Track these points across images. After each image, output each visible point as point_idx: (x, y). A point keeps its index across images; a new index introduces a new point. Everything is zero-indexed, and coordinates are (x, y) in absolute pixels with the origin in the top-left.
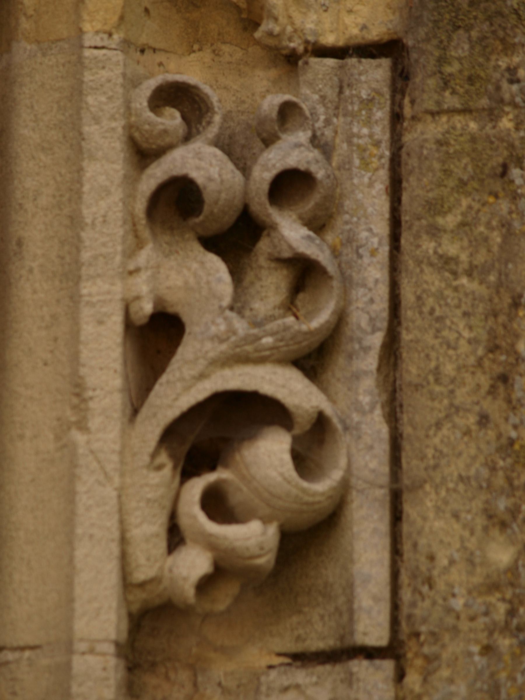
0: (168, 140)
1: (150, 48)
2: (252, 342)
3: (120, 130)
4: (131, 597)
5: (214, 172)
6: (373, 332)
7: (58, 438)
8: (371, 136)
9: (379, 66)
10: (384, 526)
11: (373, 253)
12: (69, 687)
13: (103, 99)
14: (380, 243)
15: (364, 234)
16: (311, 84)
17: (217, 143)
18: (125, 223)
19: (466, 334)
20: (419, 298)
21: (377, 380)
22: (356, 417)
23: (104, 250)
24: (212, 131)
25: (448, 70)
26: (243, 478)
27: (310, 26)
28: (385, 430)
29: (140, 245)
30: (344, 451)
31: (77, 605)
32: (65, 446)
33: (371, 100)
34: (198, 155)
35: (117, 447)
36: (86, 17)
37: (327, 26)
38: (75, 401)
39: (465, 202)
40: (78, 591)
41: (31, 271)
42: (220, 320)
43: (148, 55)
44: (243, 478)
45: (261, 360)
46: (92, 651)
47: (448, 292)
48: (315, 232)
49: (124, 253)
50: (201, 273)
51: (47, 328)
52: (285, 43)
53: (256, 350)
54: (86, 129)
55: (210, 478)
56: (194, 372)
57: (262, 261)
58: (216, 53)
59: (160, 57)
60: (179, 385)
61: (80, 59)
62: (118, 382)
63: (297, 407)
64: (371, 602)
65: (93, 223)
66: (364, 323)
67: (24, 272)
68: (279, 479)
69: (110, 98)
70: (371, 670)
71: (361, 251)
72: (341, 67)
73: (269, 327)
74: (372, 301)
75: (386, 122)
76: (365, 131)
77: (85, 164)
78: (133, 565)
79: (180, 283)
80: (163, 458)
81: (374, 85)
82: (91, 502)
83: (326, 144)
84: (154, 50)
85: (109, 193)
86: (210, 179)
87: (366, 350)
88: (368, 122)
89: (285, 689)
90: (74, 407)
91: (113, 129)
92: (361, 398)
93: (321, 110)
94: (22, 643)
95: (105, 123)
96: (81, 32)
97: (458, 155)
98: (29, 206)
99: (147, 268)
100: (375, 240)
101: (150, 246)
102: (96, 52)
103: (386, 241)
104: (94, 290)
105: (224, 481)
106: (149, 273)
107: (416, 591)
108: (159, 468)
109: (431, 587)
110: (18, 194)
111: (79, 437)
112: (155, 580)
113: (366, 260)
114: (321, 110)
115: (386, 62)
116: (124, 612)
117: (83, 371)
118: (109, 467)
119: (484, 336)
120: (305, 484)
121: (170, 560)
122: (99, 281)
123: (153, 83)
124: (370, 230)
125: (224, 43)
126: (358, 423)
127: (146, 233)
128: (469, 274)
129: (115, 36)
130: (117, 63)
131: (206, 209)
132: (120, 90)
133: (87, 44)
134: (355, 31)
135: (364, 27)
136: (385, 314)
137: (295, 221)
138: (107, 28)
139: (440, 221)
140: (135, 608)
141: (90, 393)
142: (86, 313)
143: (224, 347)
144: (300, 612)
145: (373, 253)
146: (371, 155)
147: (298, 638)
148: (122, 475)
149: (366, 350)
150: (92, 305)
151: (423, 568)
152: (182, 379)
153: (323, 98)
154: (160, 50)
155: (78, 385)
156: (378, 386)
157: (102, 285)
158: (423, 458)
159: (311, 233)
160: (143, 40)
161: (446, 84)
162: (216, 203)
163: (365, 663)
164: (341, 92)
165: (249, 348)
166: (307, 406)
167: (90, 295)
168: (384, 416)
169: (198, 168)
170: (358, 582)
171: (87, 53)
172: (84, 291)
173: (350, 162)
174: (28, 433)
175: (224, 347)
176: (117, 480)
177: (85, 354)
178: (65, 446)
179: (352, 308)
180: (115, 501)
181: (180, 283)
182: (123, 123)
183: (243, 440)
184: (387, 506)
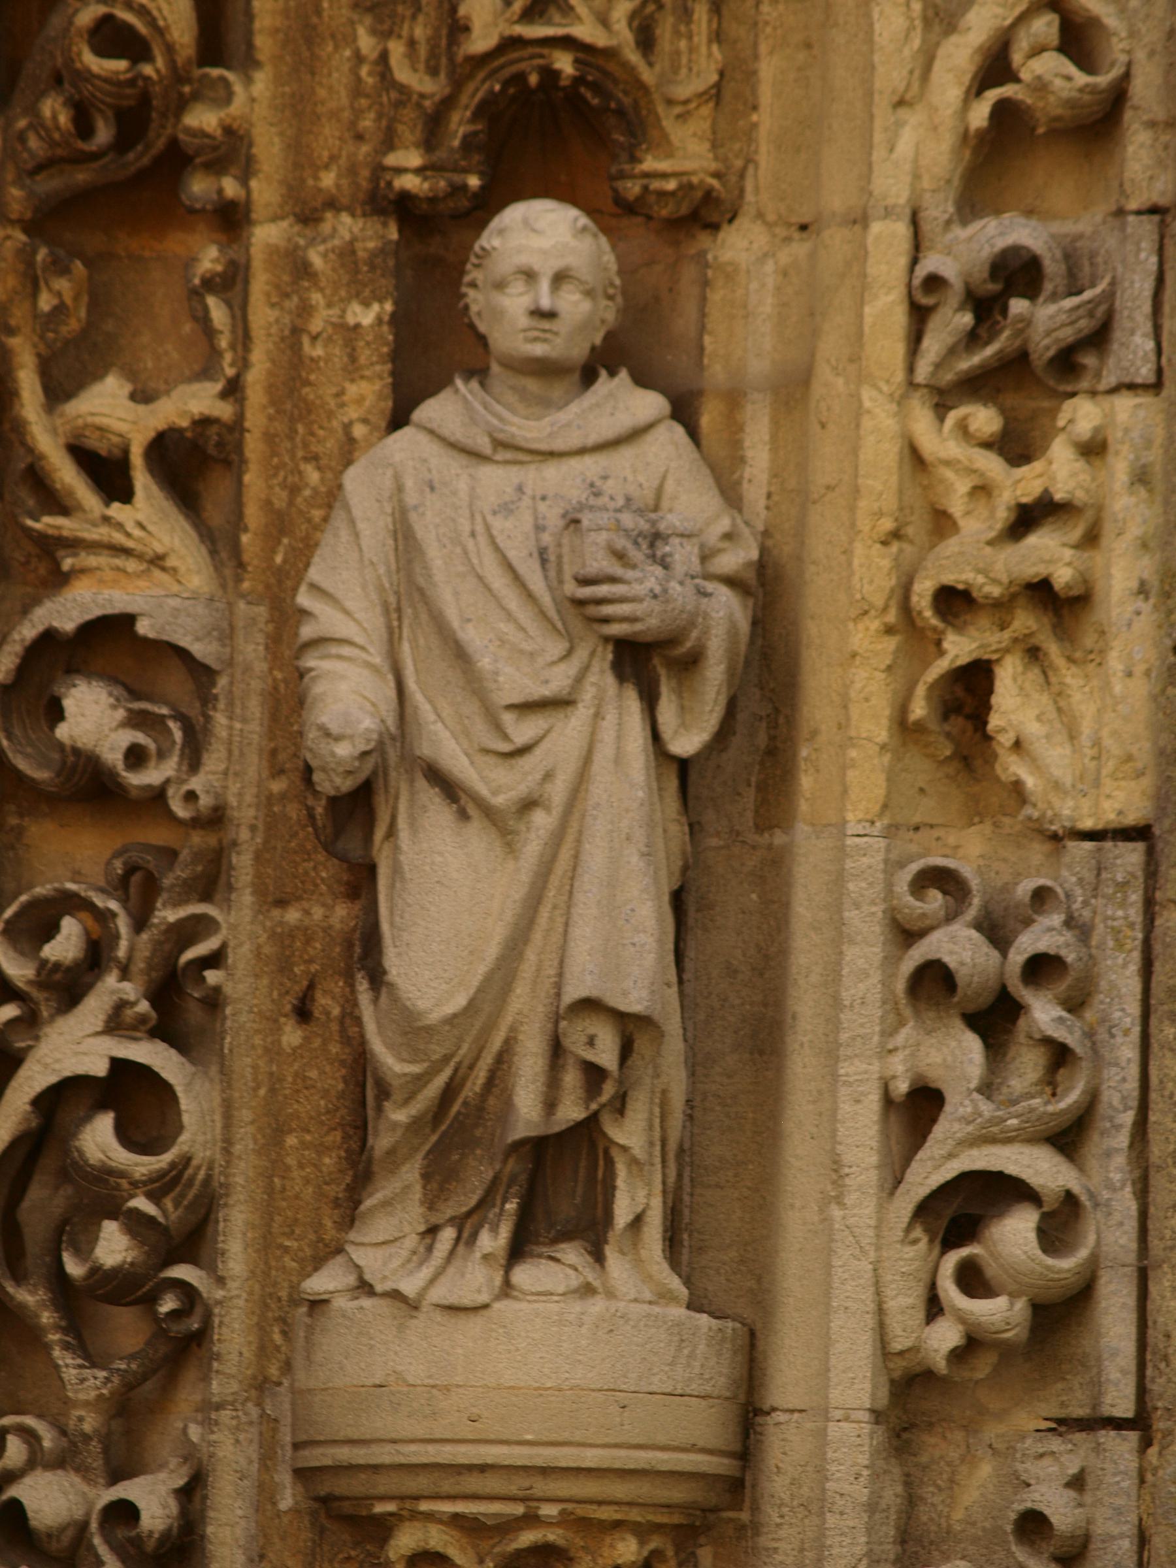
0: (928, 922)
1: (926, 825)
2: (997, 1124)
3: (880, 914)
4: (891, 1365)
5: (967, 956)
6: (1125, 1111)
7: (821, 1210)
8: (1126, 918)
9: (1134, 850)
10: (1132, 1302)
11: (1126, 1033)
12: (825, 1453)
13: (864, 885)
14: (1133, 1024)
15: (1118, 1014)
16: (1070, 867)
17: (978, 926)
18: (884, 1003)
20: (1161, 1082)
21: (1129, 1158)
22: (1106, 1194)
23: (862, 1031)
24: (972, 913)
26: (992, 1254)
27: (1066, 812)
28: (1133, 1207)
29: (902, 1023)
30: (1093, 1228)
31: (831, 1375)
32: (825, 1220)
33: (1125, 884)
34: (953, 939)
35: (873, 1222)
36: (849, 807)
37: (1085, 811)
38: (834, 1177)
40: (833, 1361)
41: (802, 1045)
42: (967, 1102)
43: (924, 833)
44: (992, 1254)
45: (1007, 1140)
46: (847, 1419)
48: (1069, 1011)
49: (883, 1033)
50: (957, 1052)
51: (814, 1102)
52: (1047, 826)
53: (1002, 1132)
54: (846, 914)
55: (964, 1252)
57: (1022, 1038)
58: (996, 825)
59: (936, 833)
60: (929, 1163)
61: (842, 848)
62: (874, 1159)
63: (1043, 1186)
64: (1118, 1375)
65: (852, 1006)
66: (1116, 1101)
67: (796, 1046)
68: (1024, 1257)
69: (871, 884)
70: (1118, 1441)
71: (1114, 1031)
72: (1099, 850)
73: (1018, 1108)
74: (1124, 1080)
75: (1140, 905)
76: (1120, 913)
77: (844, 948)
78: (891, 1335)
79: (939, 1060)
80: (918, 1232)
81: (1130, 869)
82: (846, 1276)
83: (1084, 925)
84: (932, 826)
85: (868, 976)
86: (962, 964)
87: (1118, 1127)
88: (1123, 905)
89: (1042, 1456)
90: (834, 1183)
91: (873, 914)
92: (1112, 1175)
93: (1078, 891)
94: (790, 1406)
95: (866, 908)
96: (845, 822)
98: (802, 982)
99: (905, 1047)
100: (1128, 1020)
101: (911, 1024)
102: (857, 840)
103: (1138, 1021)
104: (851, 1070)
105: (976, 1255)
106: (907, 1052)
107: (1156, 1367)
108: (915, 1242)
109: (1168, 1365)
110: (794, 970)
111: (836, 1212)
112: (914, 1349)
113: (1119, 1040)
114: (1078, 891)
115: (1140, 846)
116: (883, 1380)
117: (839, 1148)
118: (864, 1242)
120: (1050, 1261)
121: (927, 1330)
122: (856, 1062)
123: (915, 867)
124: (1123, 1010)
125: (1005, 815)
126: (1109, 1199)
127: (907, 1012)
129: (878, 824)
130: (878, 851)
131: (960, 991)
132: (881, 876)
133: (849, 832)
134: (1112, 816)
135: (1120, 813)
136: (1136, 1094)
137: (1049, 1001)
138: (869, 817)
140: (896, 1375)
141: (847, 1170)
142: (843, 1091)
143: (970, 1128)
144: (1065, 1379)
145: (1126, 1033)
146: (1126, 937)
147: (1063, 1405)
148: (878, 1248)
149: (1118, 1127)
150: (848, 1084)
151: (1161, 1346)
152: (932, 1158)
153: (1081, 880)
154: (938, 825)
155: (835, 1162)
156: (1129, 1163)
157: (860, 1065)
158: (1162, 1239)
159: (1064, 1014)
160: (917, 819)
162: (969, 985)
163: (1113, 1433)
164: (1098, 875)
165: (995, 1129)
166: (1052, 1185)
167: (847, 1075)
168: (1134, 1193)
169: (951, 953)
170: (1105, 1356)
171: (849, 841)
172: (842, 1072)
173: (1105, 943)
174: (798, 1204)
175: (970, 1128)
176: (872, 1255)
177: (842, 1131)
178: (825, 1220)
179: (1104, 1087)
180: (870, 1274)
181: (939, 1060)
182: (883, 907)
183: (994, 1217)
184: (1135, 1281)
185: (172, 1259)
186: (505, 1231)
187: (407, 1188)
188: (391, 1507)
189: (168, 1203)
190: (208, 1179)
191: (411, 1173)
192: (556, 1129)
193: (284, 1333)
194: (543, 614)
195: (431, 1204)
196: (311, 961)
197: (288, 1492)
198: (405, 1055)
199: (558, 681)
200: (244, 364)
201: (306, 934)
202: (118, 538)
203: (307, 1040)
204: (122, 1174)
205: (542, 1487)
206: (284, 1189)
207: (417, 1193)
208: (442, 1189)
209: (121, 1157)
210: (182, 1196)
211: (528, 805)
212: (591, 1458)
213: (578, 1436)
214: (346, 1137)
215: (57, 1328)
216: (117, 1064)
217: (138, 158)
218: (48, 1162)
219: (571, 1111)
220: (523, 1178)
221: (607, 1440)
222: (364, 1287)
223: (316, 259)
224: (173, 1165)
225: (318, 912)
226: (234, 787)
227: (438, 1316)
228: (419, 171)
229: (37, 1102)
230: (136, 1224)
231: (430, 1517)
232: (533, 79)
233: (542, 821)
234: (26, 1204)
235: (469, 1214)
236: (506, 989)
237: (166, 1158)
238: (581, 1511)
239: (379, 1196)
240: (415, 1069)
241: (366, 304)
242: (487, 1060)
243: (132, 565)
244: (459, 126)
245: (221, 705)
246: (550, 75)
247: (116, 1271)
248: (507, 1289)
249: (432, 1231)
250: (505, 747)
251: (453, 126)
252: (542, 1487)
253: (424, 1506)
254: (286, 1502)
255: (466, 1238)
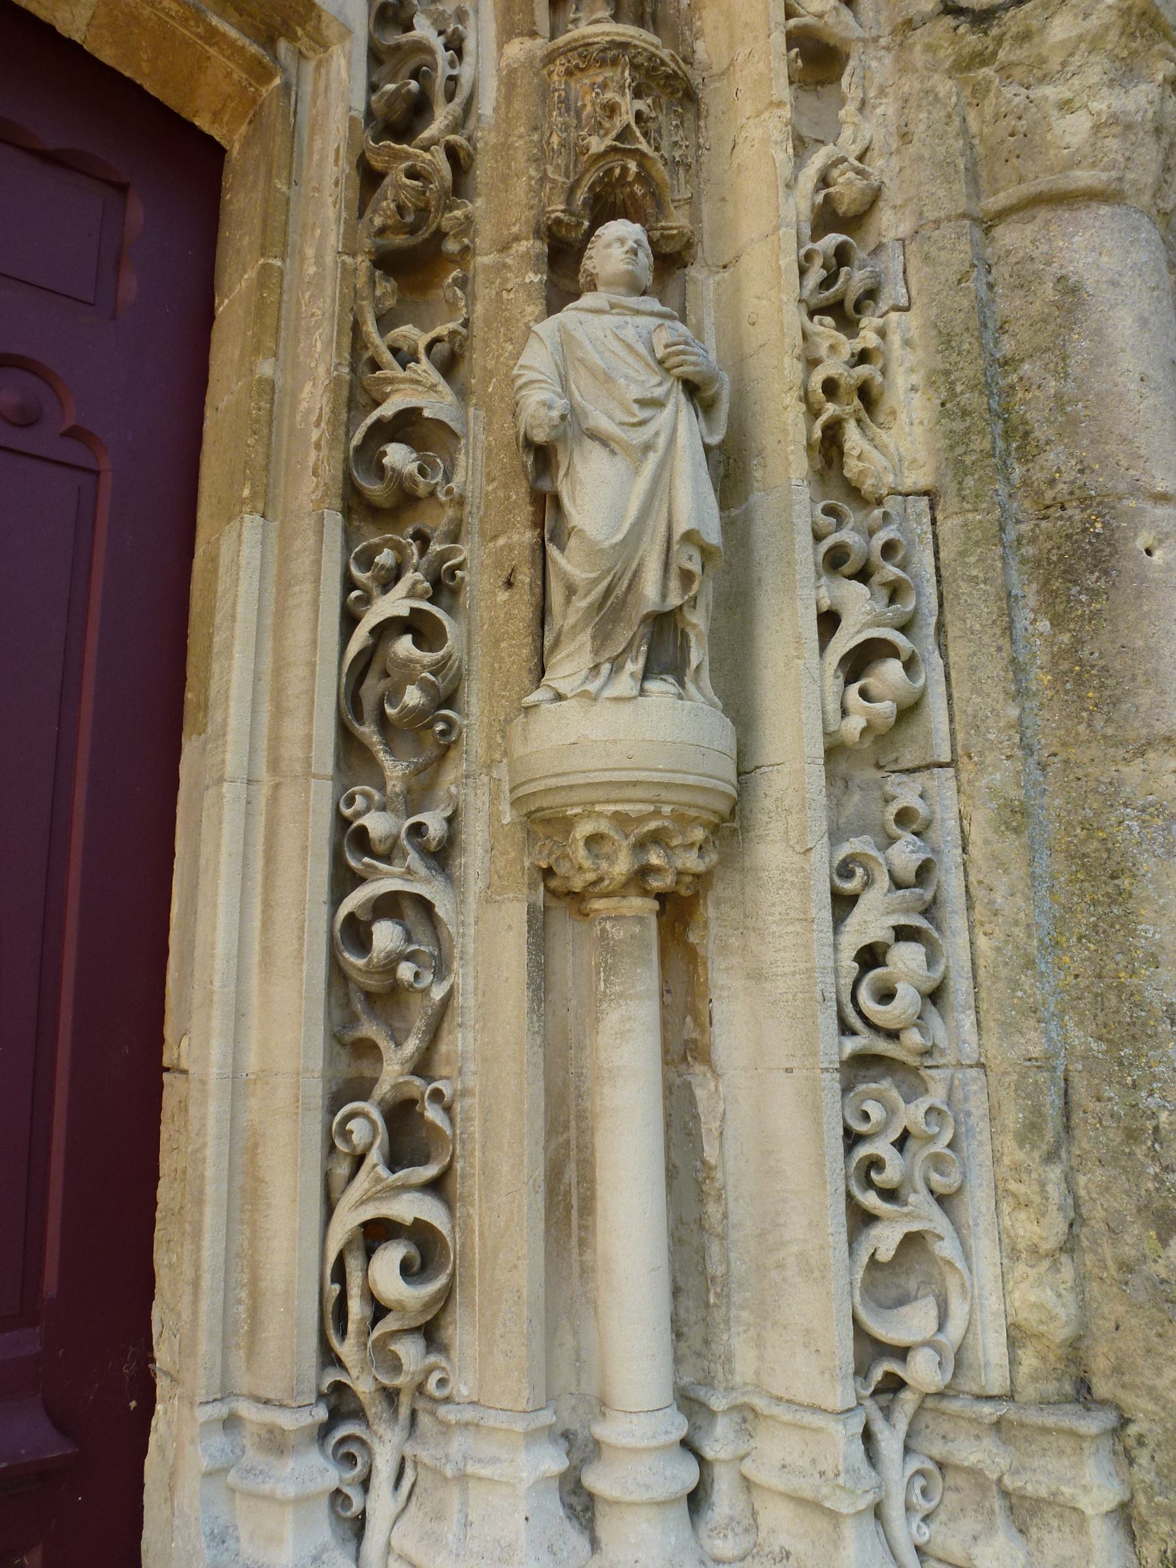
19: (986, 610)
25: (964, 493)
39: (979, 551)
46: (813, 763)
47: (974, 592)
56: (856, 630)
80: (840, 673)
97: (973, 530)
98: (764, 563)
119: (995, 609)
121: (844, 722)
128: (985, 582)
139: (967, 560)
157: (806, 592)
161: (963, 498)
185: (439, 708)
186: (641, 661)
187: (582, 645)
188: (578, 810)
189: (439, 677)
190: (459, 667)
191: (585, 637)
192: (667, 609)
193: (503, 737)
194: (648, 365)
195: (596, 652)
196: (513, 560)
197: (508, 815)
198: (587, 568)
199: (659, 392)
200: (471, 311)
201: (510, 548)
202: (415, 376)
203: (511, 596)
204: (417, 662)
205: (665, 795)
206: (500, 668)
207: (588, 647)
208: (602, 644)
209: (416, 653)
210: (447, 675)
211: (647, 447)
212: (691, 780)
213: (684, 768)
214: (534, 640)
215: (381, 743)
216: (412, 609)
217: (424, 234)
218: (375, 668)
219: (674, 601)
220: (649, 635)
221: (700, 771)
222: (559, 697)
223: (509, 261)
224: (443, 657)
225: (516, 538)
226: (470, 488)
227: (608, 704)
228: (562, 211)
229: (373, 632)
230: (425, 686)
231: (600, 814)
232: (617, 171)
233: (653, 458)
234: (364, 687)
235: (618, 656)
236: (639, 539)
237: (441, 653)
238: (683, 810)
239: (563, 654)
240: (593, 575)
241: (536, 273)
242: (629, 574)
243: (420, 388)
244: (581, 195)
245: (463, 451)
246: (625, 170)
247: (415, 708)
248: (642, 692)
249: (596, 667)
250: (635, 420)
251: (578, 196)
252: (665, 795)
253: (598, 808)
254: (507, 819)
255: (617, 665)
